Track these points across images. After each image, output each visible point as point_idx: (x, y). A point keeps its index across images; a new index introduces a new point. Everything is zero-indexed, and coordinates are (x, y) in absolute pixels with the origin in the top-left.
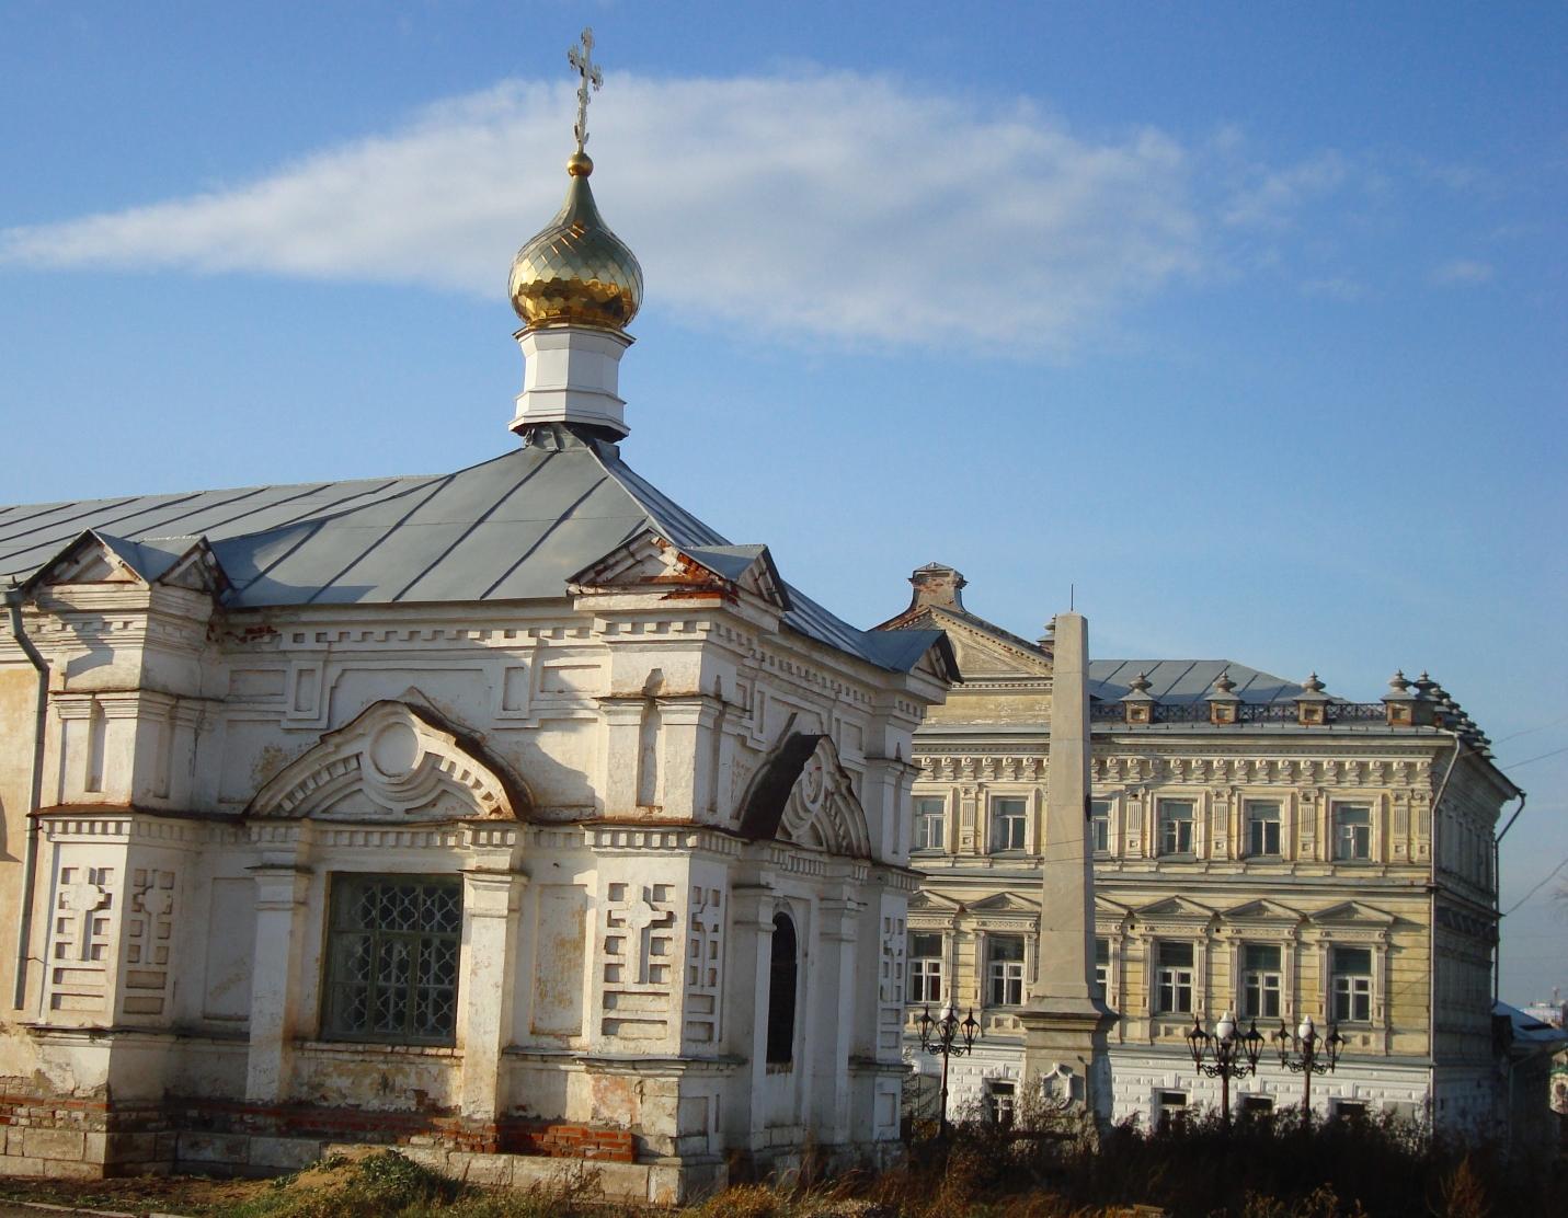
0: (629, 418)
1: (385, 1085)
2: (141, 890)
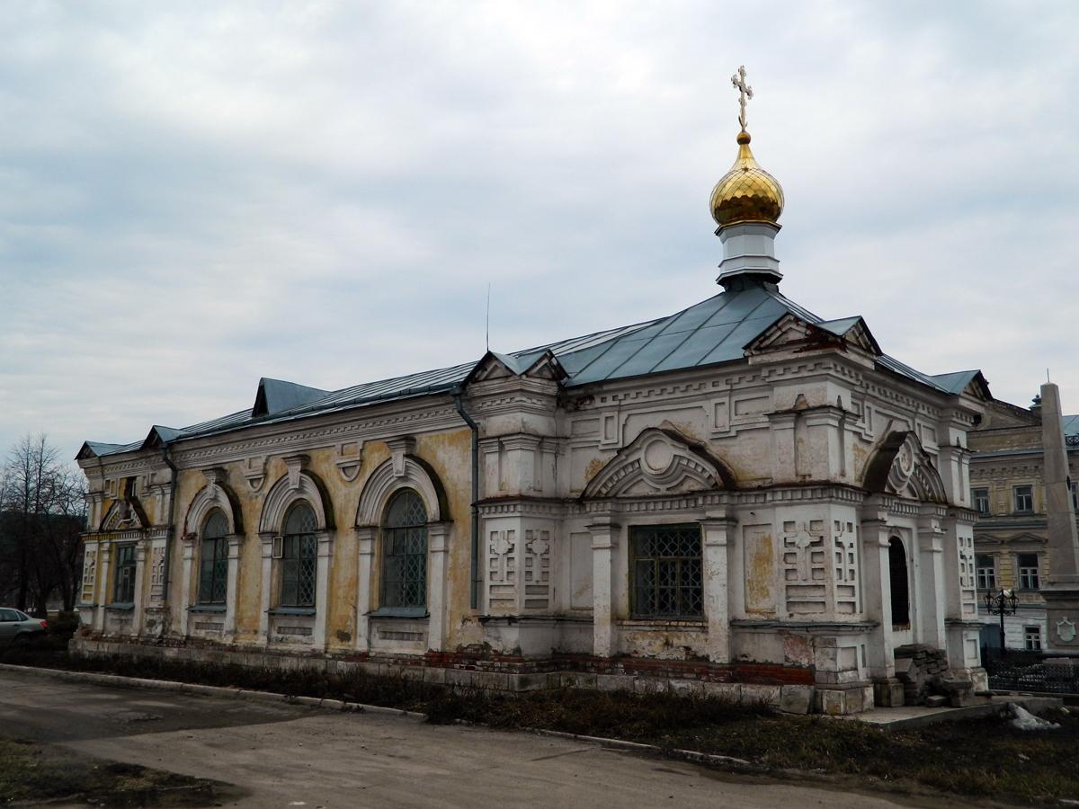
0: (781, 269)
1: (667, 644)
2: (530, 541)
